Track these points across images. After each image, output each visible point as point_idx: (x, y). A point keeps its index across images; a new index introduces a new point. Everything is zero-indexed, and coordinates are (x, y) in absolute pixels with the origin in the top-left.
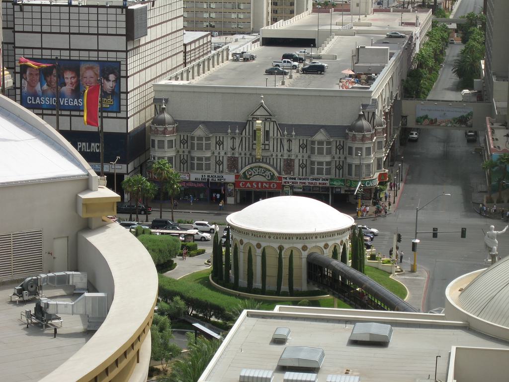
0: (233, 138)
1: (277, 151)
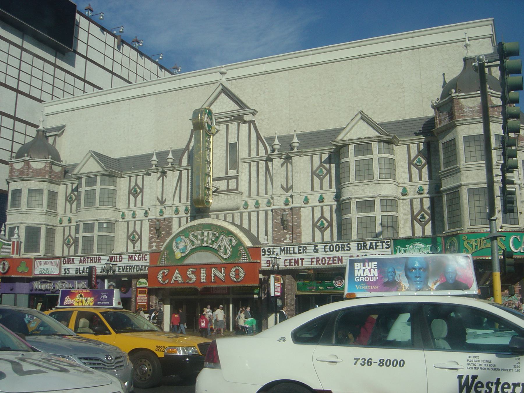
1: (258, 194)
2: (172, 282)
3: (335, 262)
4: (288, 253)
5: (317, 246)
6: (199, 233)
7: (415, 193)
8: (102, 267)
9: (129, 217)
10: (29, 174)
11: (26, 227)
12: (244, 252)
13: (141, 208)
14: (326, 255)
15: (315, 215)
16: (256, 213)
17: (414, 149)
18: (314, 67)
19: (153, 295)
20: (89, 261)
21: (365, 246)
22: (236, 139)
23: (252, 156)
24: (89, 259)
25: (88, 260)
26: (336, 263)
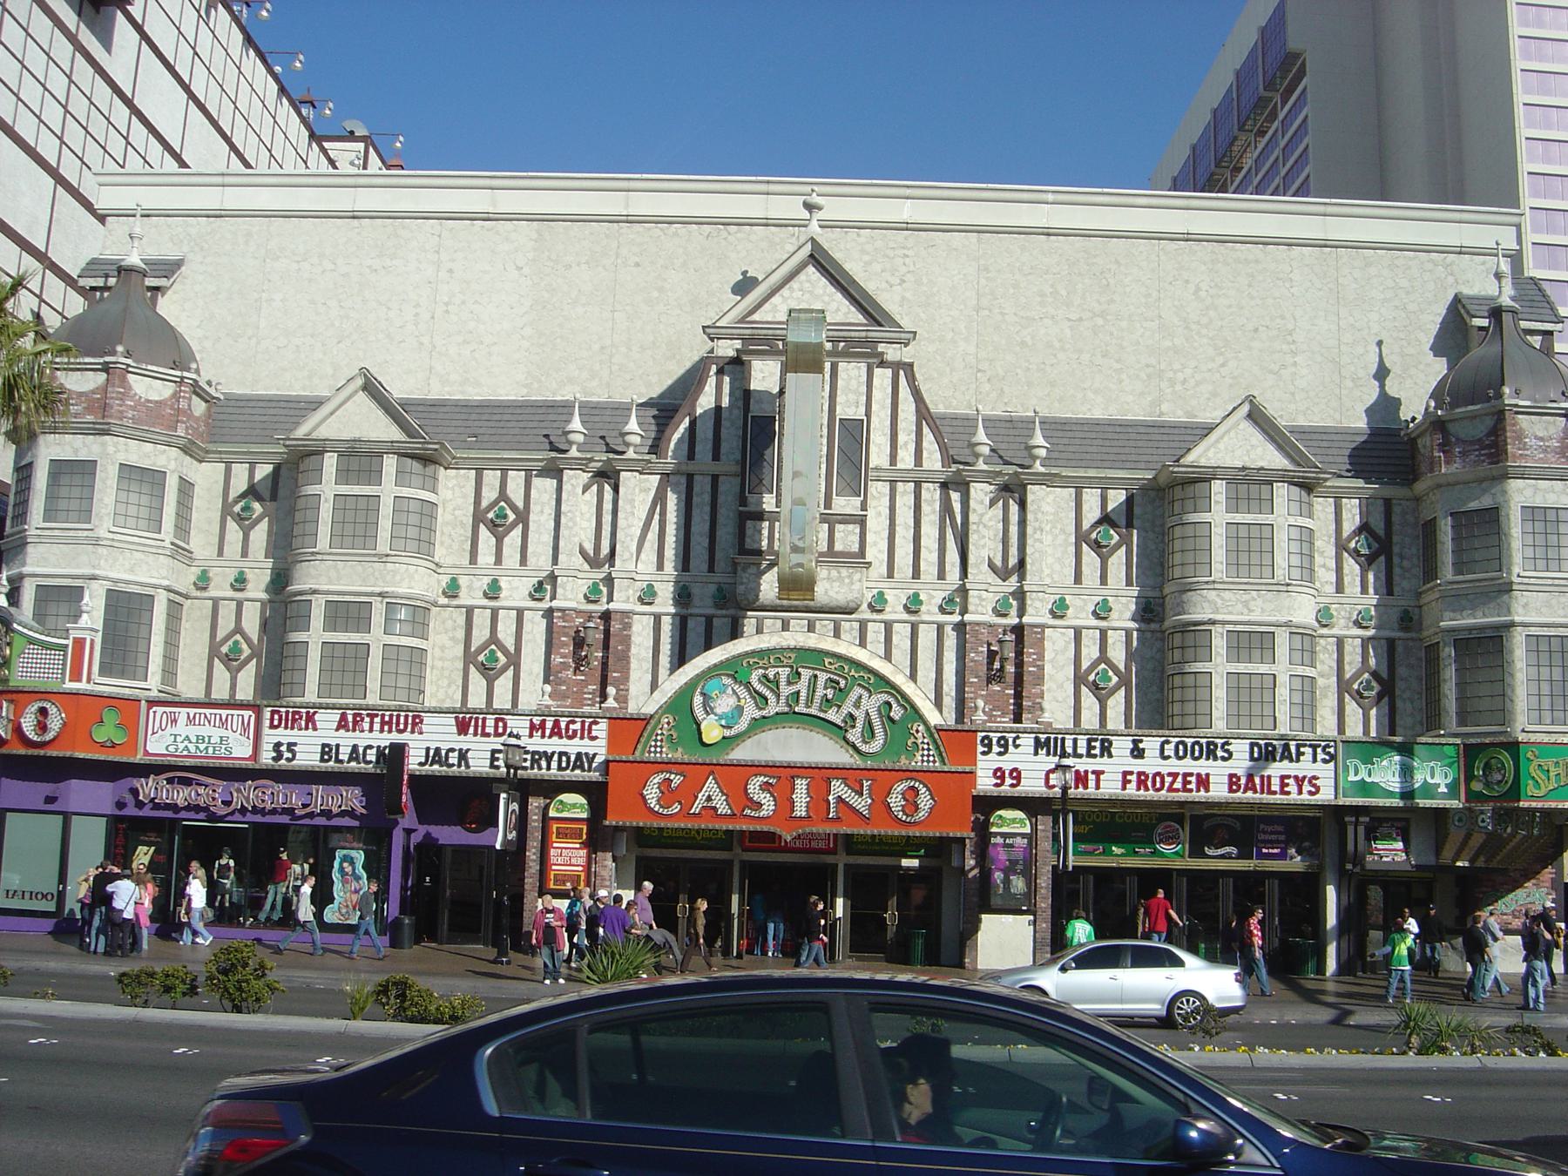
0: (607, 476)
1: (916, 574)
2: (696, 809)
3: (1188, 787)
4: (479, 732)
5: (1141, 741)
6: (784, 673)
7: (1351, 624)
8: (428, 749)
9: (472, 594)
10: (125, 414)
11: (109, 590)
12: (926, 741)
13: (937, 586)
14: (1166, 767)
15: (1084, 651)
16: (908, 627)
17: (1351, 511)
18: (1052, 237)
19: (604, 851)
20: (377, 727)
21: (294, 720)
22: (863, 410)
23: (900, 466)
24: (377, 720)
25: (372, 723)
26: (1191, 791)
